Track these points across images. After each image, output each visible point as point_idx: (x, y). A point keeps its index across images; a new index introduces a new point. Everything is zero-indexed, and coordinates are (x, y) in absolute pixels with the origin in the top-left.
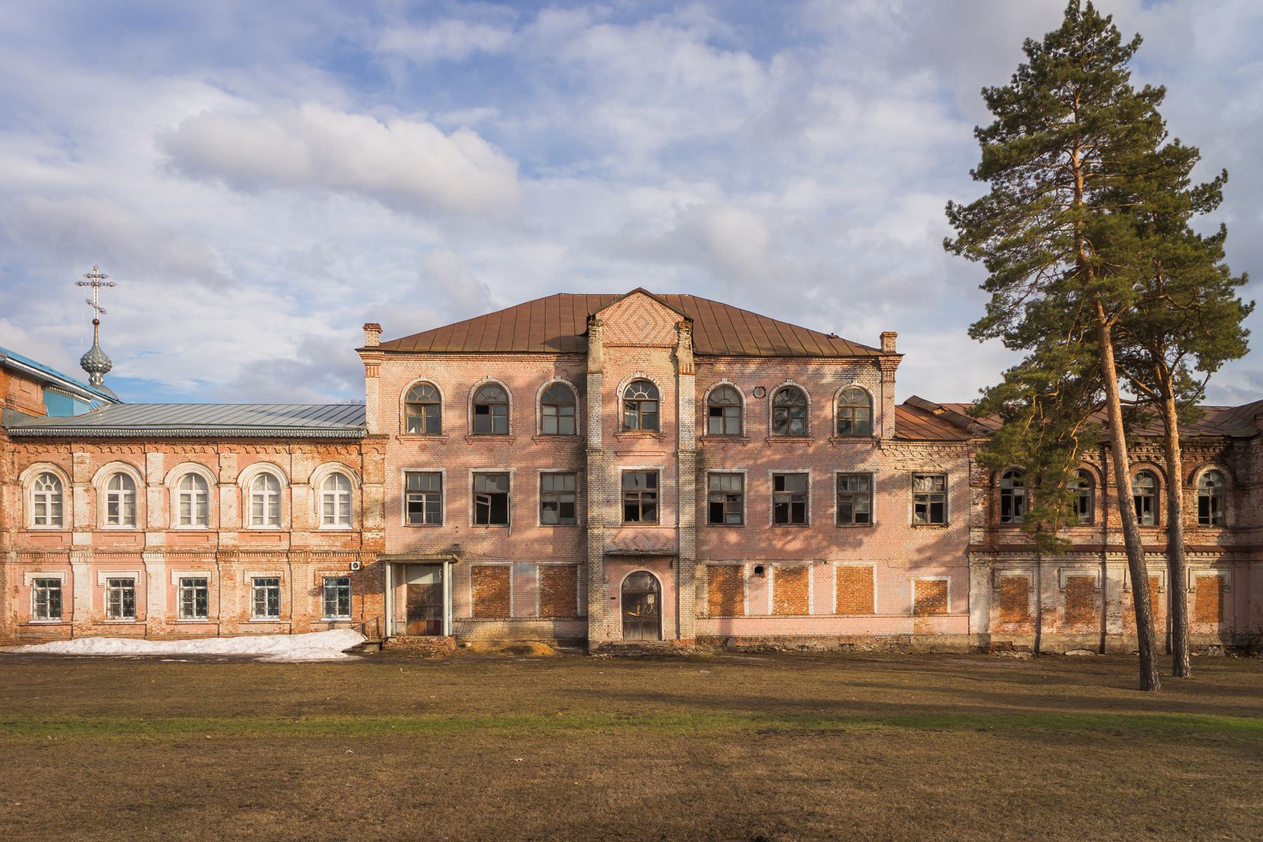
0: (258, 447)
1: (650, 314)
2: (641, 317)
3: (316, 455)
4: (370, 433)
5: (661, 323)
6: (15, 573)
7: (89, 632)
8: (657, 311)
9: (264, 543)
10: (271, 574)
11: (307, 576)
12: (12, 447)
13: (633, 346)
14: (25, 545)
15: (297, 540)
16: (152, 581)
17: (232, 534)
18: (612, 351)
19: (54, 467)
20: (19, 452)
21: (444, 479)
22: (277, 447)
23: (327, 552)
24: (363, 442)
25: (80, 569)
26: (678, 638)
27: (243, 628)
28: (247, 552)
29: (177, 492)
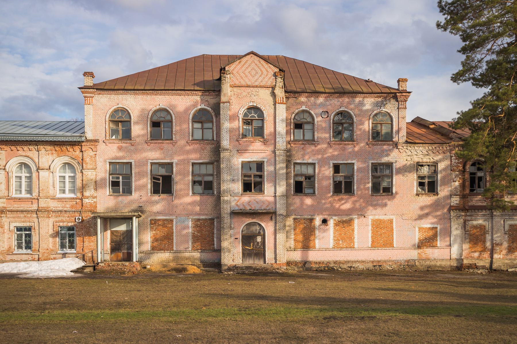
3: (54, 152)
5: (265, 72)
8: (263, 65)
9: (22, 205)
10: (27, 224)
11: (48, 225)
15: (43, 204)
18: (235, 89)
21: (133, 167)
22: (30, 147)
24: (83, 144)
26: (276, 262)
27: (9, 257)
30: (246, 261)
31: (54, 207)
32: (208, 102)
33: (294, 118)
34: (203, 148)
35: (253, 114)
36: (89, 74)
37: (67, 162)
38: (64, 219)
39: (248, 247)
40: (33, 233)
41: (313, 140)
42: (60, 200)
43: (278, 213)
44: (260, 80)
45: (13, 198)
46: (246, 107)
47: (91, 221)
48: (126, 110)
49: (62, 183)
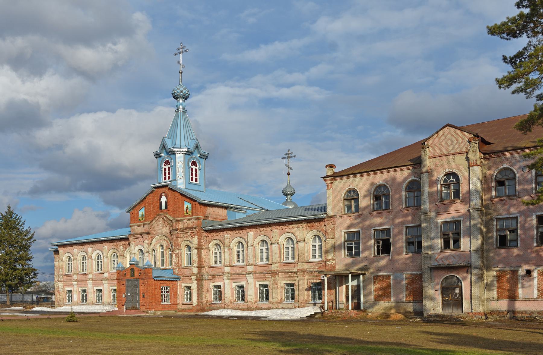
0: (286, 226)
1: (454, 136)
2: (450, 139)
3: (308, 228)
4: (329, 215)
5: (460, 140)
6: (207, 284)
7: (229, 307)
8: (457, 134)
9: (288, 268)
10: (292, 282)
11: (304, 282)
12: (206, 234)
13: (445, 155)
14: (211, 272)
15: (301, 266)
16: (249, 286)
17: (276, 265)
18: (434, 160)
19: (219, 241)
20: (209, 236)
21: (361, 234)
22: (293, 226)
23: (312, 271)
24: (326, 220)
25: (226, 281)
26: (472, 311)
27: (281, 306)
28: (282, 273)
29: (258, 248)
30: (445, 310)
31: (307, 269)
32: (418, 173)
33: (496, 176)
34: (414, 213)
35: (451, 179)
36: (332, 166)
37: (316, 234)
38: (314, 277)
39: (447, 297)
40: (269, 289)
41: (515, 195)
42: (311, 263)
43: (473, 266)
44: (455, 148)
45: (283, 263)
46: (443, 174)
47: (331, 278)
48: (355, 190)
49: (320, 250)
